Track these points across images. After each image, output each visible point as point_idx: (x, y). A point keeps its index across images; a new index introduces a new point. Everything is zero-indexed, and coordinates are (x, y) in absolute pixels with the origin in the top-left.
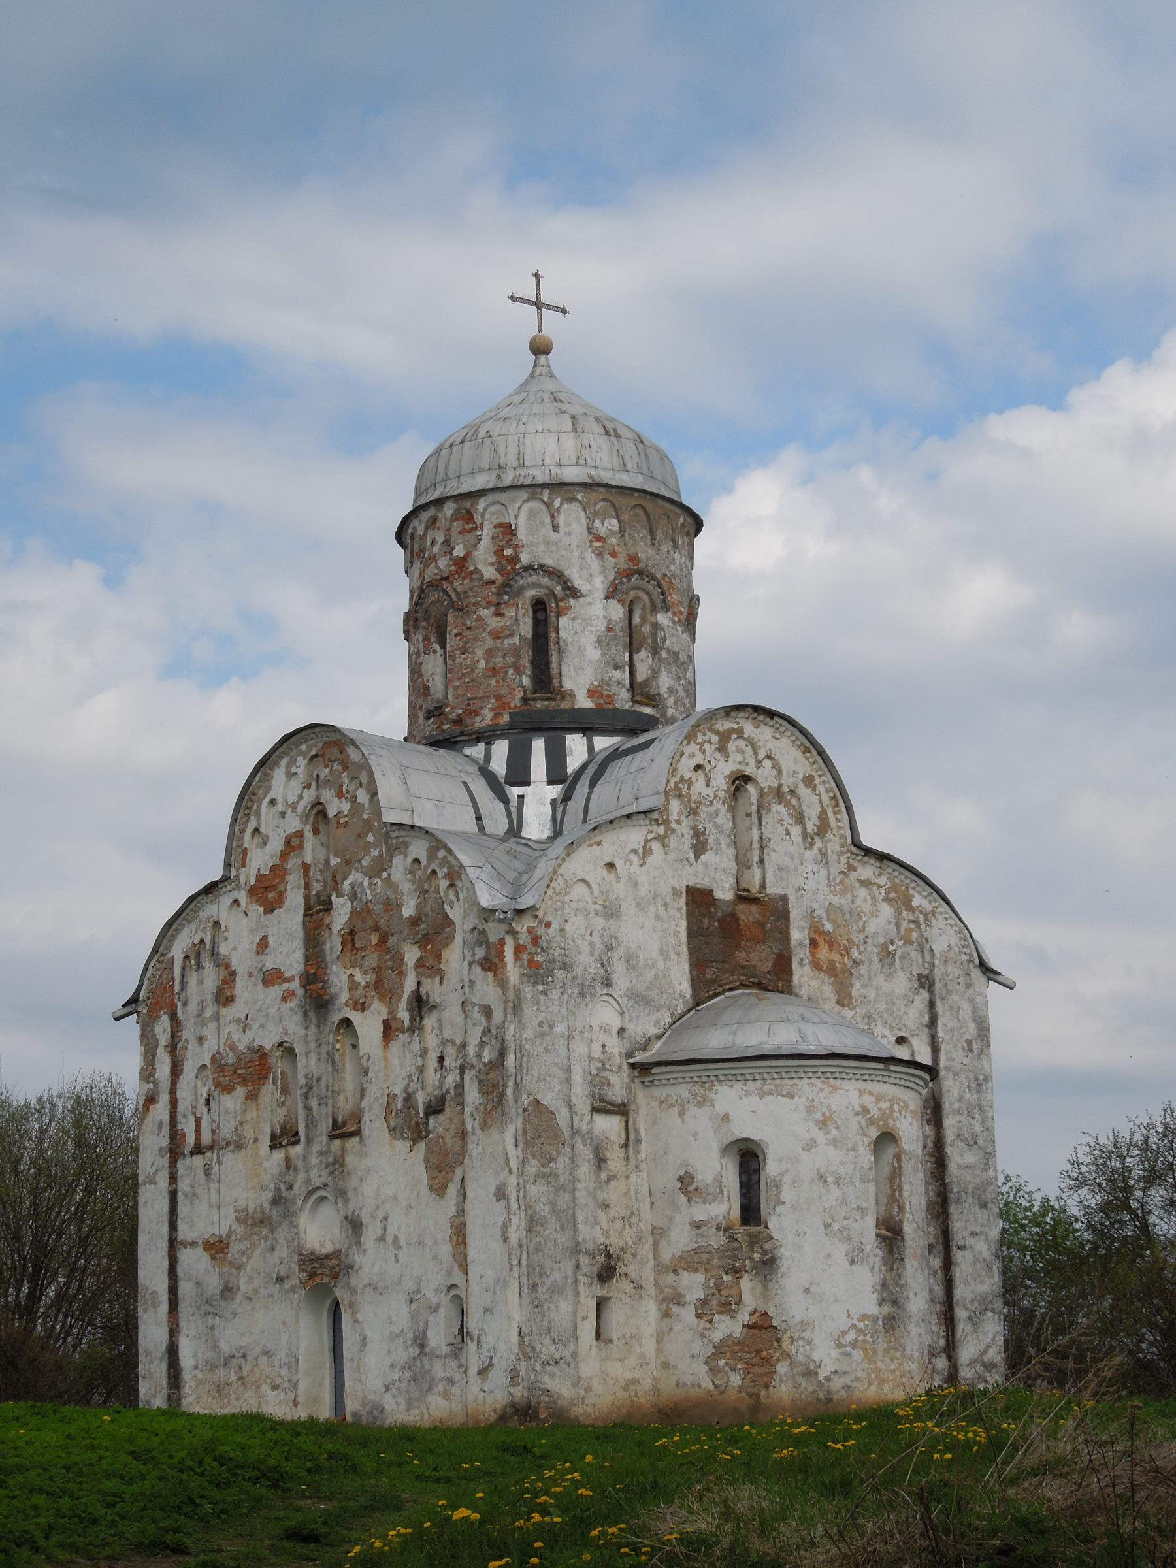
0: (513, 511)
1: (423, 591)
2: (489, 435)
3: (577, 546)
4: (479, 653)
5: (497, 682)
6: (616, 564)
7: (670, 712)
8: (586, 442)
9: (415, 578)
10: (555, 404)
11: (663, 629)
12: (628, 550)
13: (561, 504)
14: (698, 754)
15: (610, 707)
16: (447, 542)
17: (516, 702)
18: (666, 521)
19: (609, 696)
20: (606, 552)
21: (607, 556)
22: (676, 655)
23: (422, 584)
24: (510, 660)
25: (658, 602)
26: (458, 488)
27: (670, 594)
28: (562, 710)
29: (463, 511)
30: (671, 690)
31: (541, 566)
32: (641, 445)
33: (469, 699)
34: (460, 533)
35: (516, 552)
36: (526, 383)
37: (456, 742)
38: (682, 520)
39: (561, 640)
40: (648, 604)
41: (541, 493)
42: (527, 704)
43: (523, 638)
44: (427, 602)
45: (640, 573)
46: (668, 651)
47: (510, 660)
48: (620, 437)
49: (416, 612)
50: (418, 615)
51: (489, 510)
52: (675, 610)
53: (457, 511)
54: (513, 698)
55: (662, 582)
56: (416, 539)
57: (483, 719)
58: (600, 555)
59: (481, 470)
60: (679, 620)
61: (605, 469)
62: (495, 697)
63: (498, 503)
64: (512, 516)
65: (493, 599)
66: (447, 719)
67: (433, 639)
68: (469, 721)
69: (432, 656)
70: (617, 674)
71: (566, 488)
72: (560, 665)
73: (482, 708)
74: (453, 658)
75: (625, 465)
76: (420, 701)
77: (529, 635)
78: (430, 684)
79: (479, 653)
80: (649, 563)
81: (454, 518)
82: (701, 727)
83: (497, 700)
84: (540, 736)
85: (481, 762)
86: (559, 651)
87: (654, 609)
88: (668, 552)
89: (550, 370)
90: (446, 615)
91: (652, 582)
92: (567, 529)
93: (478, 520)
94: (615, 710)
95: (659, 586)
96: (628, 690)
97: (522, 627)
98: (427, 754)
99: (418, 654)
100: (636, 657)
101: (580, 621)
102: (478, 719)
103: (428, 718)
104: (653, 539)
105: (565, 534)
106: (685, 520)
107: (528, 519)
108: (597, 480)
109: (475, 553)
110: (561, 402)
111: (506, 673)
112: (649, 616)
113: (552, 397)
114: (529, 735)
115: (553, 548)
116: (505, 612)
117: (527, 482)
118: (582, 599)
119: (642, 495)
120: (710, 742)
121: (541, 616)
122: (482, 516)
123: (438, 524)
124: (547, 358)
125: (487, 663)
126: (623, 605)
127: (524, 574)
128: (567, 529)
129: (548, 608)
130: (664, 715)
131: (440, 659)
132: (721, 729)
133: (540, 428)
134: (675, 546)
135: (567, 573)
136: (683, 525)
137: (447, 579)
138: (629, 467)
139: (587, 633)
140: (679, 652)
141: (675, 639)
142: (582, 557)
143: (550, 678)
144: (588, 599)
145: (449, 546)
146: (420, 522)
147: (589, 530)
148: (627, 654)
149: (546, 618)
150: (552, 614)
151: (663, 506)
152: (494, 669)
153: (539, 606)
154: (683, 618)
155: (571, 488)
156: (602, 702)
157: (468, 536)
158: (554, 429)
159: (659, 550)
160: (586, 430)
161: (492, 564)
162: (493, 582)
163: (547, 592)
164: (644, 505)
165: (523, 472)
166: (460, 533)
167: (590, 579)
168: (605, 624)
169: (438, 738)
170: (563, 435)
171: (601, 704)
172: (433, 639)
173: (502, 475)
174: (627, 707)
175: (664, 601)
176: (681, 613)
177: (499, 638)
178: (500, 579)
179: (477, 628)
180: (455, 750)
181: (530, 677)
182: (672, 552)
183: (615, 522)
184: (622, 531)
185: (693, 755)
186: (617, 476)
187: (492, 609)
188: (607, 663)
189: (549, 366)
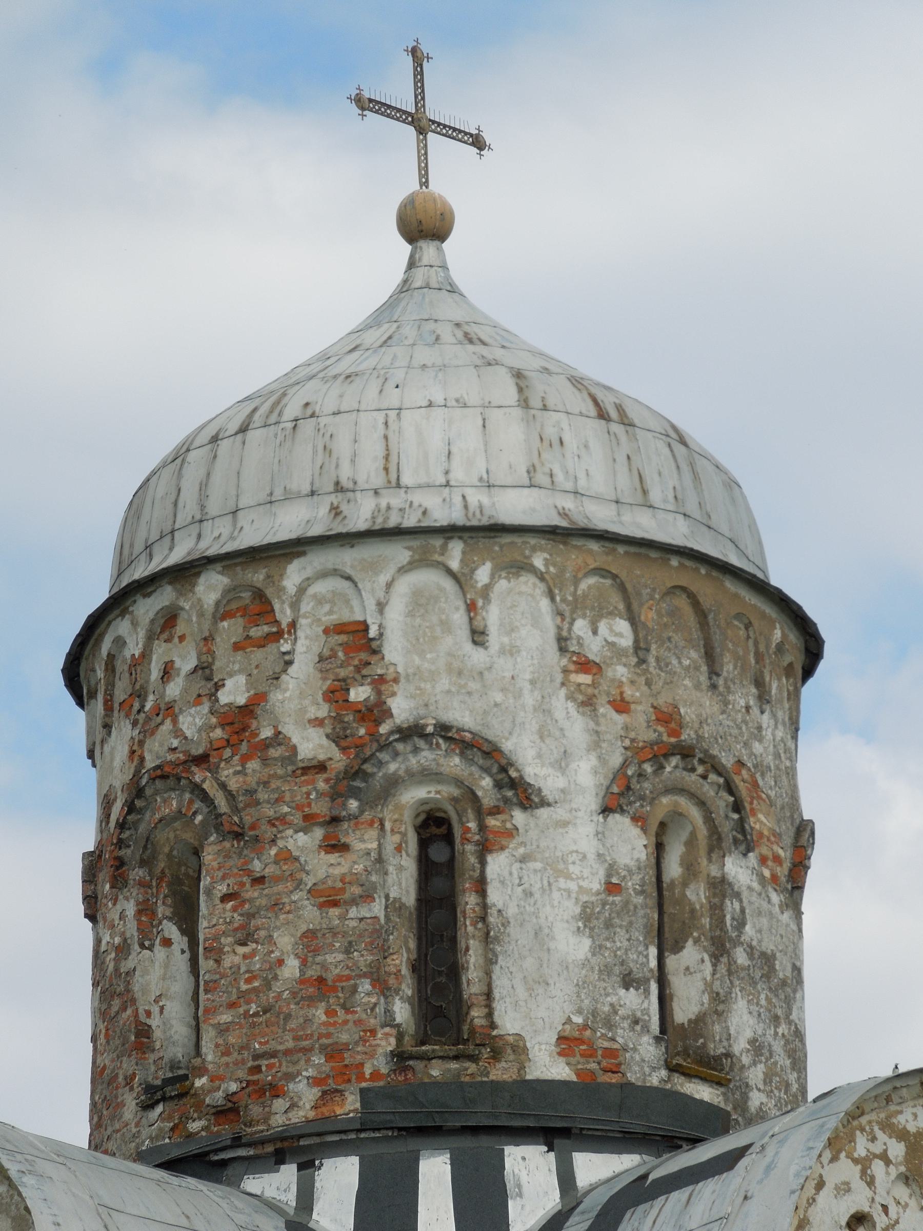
0: (373, 591)
1: (139, 792)
2: (310, 412)
3: (533, 682)
4: (285, 941)
5: (330, 1013)
6: (626, 728)
7: (756, 1099)
8: (551, 432)
9: (117, 763)
10: (470, 348)
11: (737, 895)
12: (655, 696)
13: (492, 576)
14: (858, 1185)
15: (614, 1079)
16: (204, 670)
17: (379, 1063)
18: (742, 633)
19: (610, 1053)
20: (603, 699)
21: (604, 709)
22: (768, 959)
23: (137, 775)
24: (363, 958)
25: (727, 829)
26: (232, 538)
27: (753, 812)
28: (497, 1086)
29: (246, 595)
30: (757, 1047)
31: (443, 729)
32: (682, 449)
33: (256, 1057)
34: (237, 647)
35: (379, 693)
36: (391, 304)
37: (224, 1164)
38: (777, 634)
39: (493, 912)
40: (703, 832)
41: (444, 550)
42: (405, 1069)
43: (394, 906)
44: (149, 819)
45: (686, 753)
46: (751, 950)
47: (363, 958)
48: (632, 425)
49: (121, 844)
50: (126, 853)
51: (311, 591)
52: (765, 851)
53: (230, 593)
54: (371, 1055)
55: (737, 779)
56: (121, 667)
57: (293, 1106)
58: (588, 704)
59: (290, 497)
60: (774, 878)
61: (596, 498)
62: (323, 1049)
63: (336, 573)
64: (371, 605)
65: (321, 808)
66: (199, 1105)
67: (162, 910)
68: (255, 1110)
69: (160, 952)
70: (630, 999)
71: (507, 539)
72: (488, 974)
73: (290, 1077)
74: (216, 953)
75: (645, 492)
76: (128, 1065)
77: (410, 899)
78: (155, 1022)
79: (285, 941)
80: (707, 731)
81: (223, 613)
82: (864, 1120)
83: (329, 1058)
84: (439, 1149)
85: (291, 1212)
86: (487, 939)
87: (716, 844)
88: (748, 708)
89: (448, 278)
90: (197, 852)
91: (713, 777)
92: (506, 640)
93: (284, 615)
94: (627, 1086)
95: (730, 788)
96: (658, 1040)
97: (392, 877)
98: (158, 1182)
99: (123, 950)
100: (671, 961)
101: (538, 865)
102: (279, 1104)
103: (147, 1107)
104: (714, 672)
105: (502, 652)
106: (784, 635)
107: (411, 614)
108: (582, 522)
109: (276, 697)
110: (484, 343)
111: (354, 990)
112: (704, 862)
113: (460, 334)
114: (412, 1143)
115: (473, 686)
116: (351, 839)
117: (411, 521)
118: (543, 812)
119: (688, 563)
120: (884, 1157)
121: (438, 853)
122: (295, 605)
123: (180, 628)
124: (440, 250)
125: (304, 963)
126: (644, 830)
127: (400, 746)
128: (506, 640)
129: (457, 832)
130: (742, 1105)
131: (181, 962)
132: (912, 1128)
133: (439, 399)
134: (763, 698)
135: (507, 746)
136: (780, 648)
137: (202, 760)
138: (655, 496)
139: (556, 895)
140: (774, 956)
141: (764, 921)
142: (543, 709)
143: (460, 1007)
144: (560, 813)
145: (209, 679)
146: (135, 624)
147: (562, 643)
148: (653, 951)
149: (452, 859)
150: (469, 848)
151: (736, 596)
152: (321, 980)
153: (434, 830)
154: (782, 872)
155: (517, 539)
156: (593, 1066)
157: (258, 655)
158: (473, 398)
159: (726, 703)
160: (550, 403)
161: (318, 722)
162: (321, 767)
163: (456, 792)
164: (693, 588)
165: (396, 500)
166: (237, 647)
167: (563, 762)
168: (602, 874)
169: (175, 1153)
170: (495, 415)
171: (592, 1072)
172: (162, 910)
173: (344, 507)
174: (654, 1080)
175: (741, 826)
176: (777, 859)
177: (335, 904)
178: (338, 759)
179: (277, 879)
180: (218, 1181)
181: (410, 1000)
182: (755, 711)
183: (623, 626)
184: (640, 649)
185: (844, 1188)
186: (627, 517)
187: (318, 833)
188: (607, 970)
189: (444, 267)
